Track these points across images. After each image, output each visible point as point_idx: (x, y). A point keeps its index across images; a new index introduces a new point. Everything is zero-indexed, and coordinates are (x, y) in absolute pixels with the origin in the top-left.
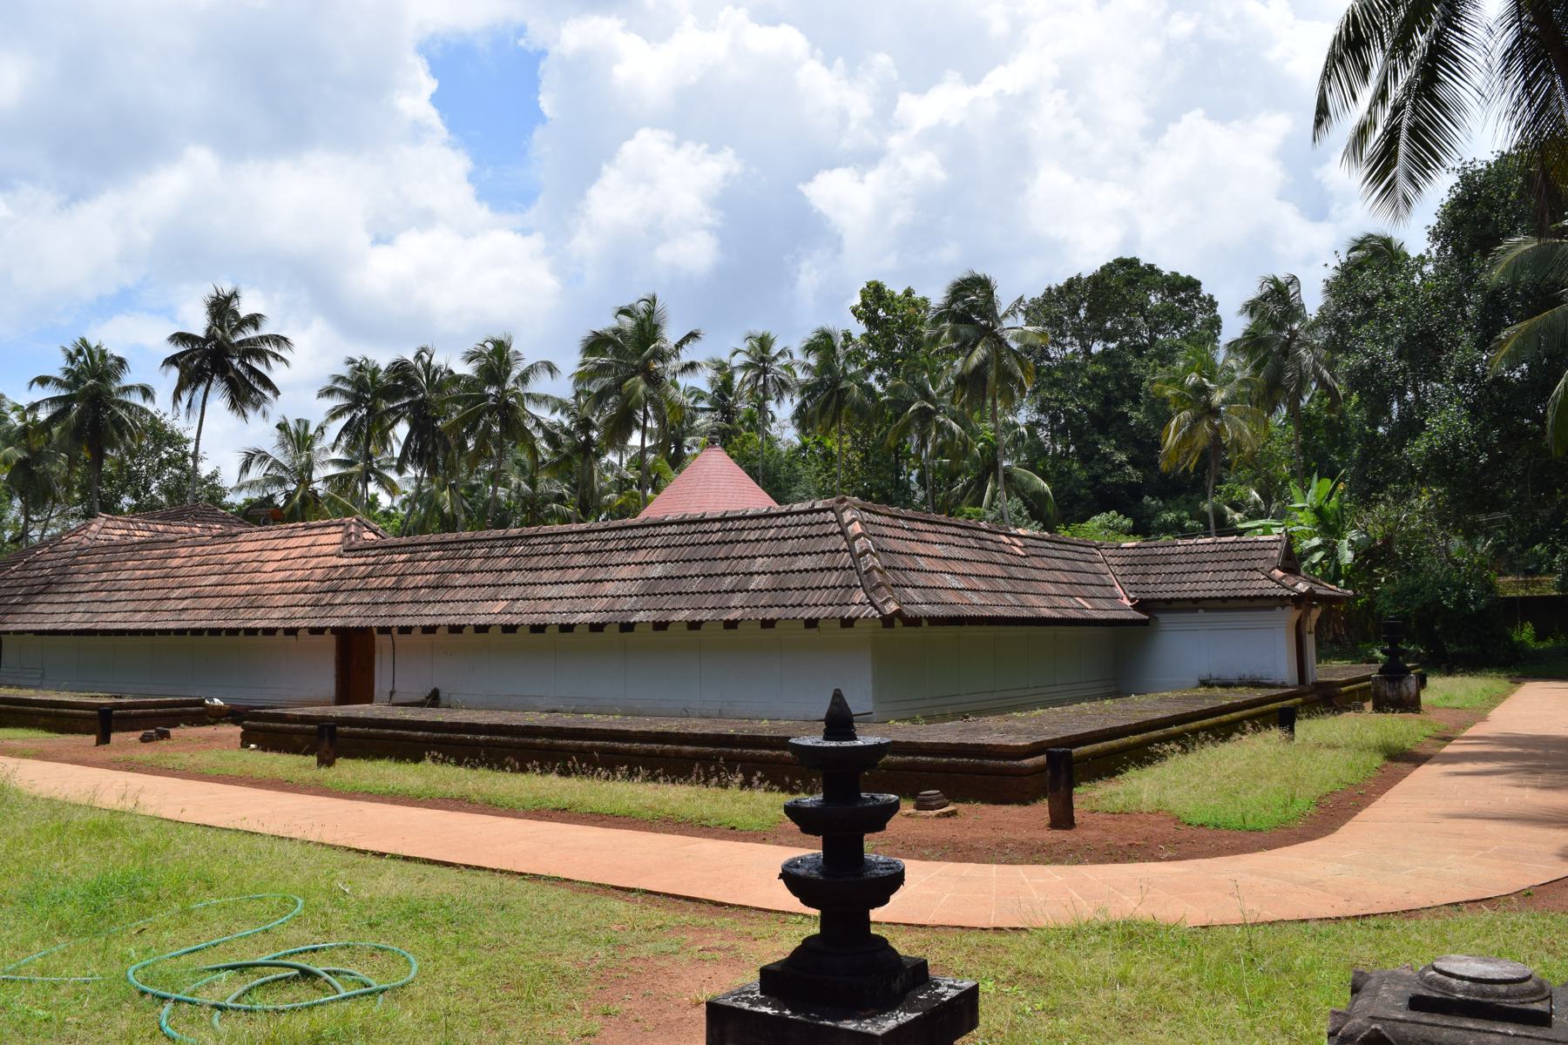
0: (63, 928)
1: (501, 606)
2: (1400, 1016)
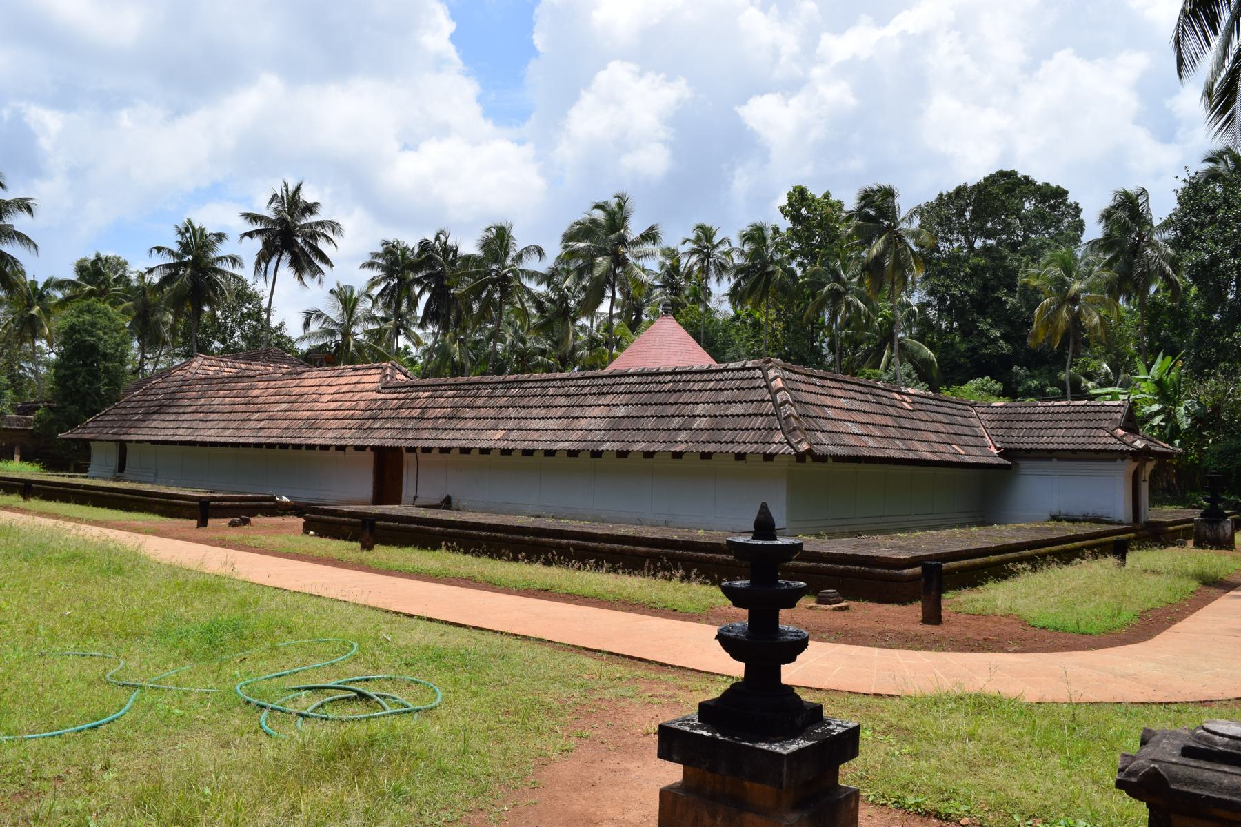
0: (188, 654)
1: (500, 434)
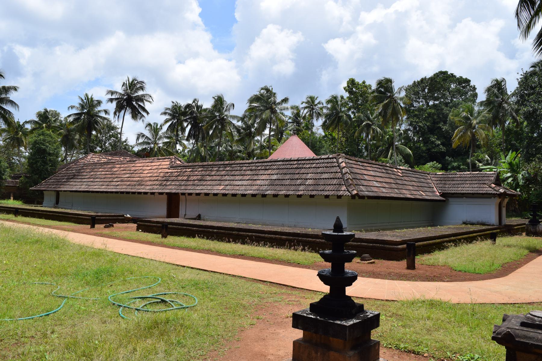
0: (88, 283)
1: (222, 187)
2: (517, 328)
